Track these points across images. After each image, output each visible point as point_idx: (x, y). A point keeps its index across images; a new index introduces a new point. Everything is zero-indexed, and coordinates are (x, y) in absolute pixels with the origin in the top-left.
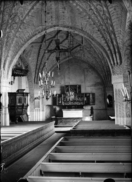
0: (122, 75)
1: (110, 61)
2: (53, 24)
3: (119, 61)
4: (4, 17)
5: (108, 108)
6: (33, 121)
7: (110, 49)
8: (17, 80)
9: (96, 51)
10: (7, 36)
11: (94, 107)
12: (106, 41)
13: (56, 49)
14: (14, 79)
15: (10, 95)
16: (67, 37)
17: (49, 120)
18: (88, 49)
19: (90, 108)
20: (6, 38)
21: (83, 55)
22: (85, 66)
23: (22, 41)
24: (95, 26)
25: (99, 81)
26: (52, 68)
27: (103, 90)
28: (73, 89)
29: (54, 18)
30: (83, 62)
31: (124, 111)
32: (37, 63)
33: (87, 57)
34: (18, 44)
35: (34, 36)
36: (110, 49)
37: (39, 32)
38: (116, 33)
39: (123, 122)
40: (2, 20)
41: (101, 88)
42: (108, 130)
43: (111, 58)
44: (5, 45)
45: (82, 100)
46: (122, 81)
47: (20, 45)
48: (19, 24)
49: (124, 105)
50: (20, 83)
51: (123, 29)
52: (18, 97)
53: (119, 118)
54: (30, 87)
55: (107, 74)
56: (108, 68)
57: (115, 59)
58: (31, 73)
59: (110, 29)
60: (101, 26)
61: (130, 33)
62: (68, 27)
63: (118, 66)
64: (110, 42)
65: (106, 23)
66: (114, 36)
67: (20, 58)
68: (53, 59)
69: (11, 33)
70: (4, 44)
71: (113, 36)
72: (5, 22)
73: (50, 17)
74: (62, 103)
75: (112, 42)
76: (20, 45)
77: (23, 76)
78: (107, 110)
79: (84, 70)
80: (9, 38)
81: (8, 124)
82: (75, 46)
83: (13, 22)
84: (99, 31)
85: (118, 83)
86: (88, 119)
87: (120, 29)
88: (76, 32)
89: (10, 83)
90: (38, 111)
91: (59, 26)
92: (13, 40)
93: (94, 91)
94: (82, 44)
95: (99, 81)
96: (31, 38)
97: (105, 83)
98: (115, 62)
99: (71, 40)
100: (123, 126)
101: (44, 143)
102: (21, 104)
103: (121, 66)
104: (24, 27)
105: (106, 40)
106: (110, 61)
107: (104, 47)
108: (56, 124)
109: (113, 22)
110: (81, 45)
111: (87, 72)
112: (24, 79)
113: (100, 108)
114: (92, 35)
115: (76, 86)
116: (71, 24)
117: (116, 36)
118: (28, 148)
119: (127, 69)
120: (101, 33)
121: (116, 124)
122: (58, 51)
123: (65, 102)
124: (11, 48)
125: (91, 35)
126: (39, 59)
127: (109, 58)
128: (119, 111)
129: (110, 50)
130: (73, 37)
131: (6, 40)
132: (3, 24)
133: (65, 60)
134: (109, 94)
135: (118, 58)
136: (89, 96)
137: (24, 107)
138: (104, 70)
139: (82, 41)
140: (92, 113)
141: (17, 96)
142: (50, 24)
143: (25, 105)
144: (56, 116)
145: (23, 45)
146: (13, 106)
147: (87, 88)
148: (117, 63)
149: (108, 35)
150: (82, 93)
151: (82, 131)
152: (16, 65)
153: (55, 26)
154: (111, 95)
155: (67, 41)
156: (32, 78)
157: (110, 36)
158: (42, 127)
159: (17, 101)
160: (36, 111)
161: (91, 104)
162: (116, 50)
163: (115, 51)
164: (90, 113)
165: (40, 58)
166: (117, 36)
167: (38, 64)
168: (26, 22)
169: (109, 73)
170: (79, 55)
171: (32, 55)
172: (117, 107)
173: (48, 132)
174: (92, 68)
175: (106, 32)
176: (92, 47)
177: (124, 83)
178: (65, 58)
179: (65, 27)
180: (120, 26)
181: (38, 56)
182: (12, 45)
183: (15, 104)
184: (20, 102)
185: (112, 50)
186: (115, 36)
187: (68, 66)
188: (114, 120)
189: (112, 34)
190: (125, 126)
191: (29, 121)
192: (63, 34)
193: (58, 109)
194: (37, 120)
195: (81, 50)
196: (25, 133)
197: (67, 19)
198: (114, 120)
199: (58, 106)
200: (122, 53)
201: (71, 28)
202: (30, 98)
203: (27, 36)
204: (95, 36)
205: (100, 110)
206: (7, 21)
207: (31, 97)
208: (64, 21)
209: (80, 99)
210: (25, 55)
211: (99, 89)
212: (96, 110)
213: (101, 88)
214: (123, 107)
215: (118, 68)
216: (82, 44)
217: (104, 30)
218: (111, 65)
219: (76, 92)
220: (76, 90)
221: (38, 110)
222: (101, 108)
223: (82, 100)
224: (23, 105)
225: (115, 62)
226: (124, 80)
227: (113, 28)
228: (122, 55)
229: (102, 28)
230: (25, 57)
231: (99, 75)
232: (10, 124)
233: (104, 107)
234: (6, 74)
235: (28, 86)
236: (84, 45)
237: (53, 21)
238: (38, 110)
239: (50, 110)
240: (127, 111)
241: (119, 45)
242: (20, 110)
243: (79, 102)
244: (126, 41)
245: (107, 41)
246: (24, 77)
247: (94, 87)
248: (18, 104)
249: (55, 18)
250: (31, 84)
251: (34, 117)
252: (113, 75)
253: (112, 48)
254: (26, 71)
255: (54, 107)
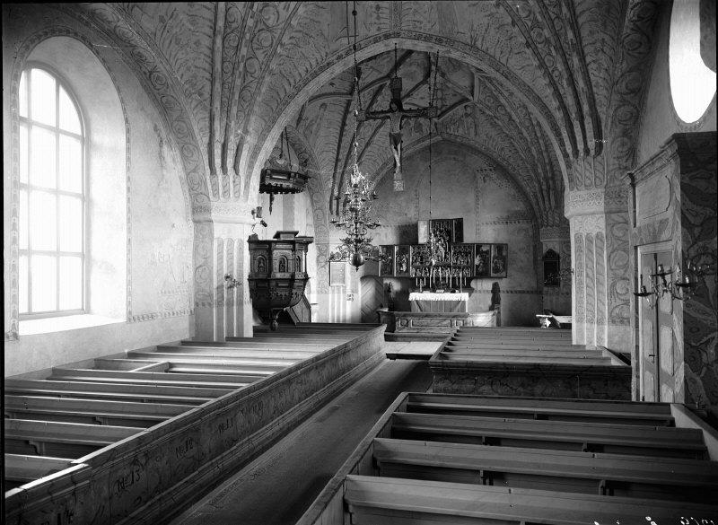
0: (601, 191)
1: (562, 144)
2: (383, 31)
3: (592, 143)
4: (231, 10)
5: (545, 289)
6: (324, 322)
7: (563, 107)
8: (281, 204)
9: (514, 117)
10: (241, 69)
11: (503, 284)
12: (551, 79)
13: (391, 110)
14: (272, 199)
15: (255, 249)
16: (428, 75)
17: (367, 321)
18: (488, 112)
19: (490, 288)
20: (239, 77)
21: (472, 130)
22: (477, 162)
23: (287, 87)
24: (516, 29)
25: (520, 206)
26: (382, 169)
27: (531, 233)
28: (441, 232)
29: (385, 11)
30: (474, 150)
31: (604, 305)
32: (338, 154)
33: (485, 136)
34: (275, 95)
35: (322, 69)
36: (563, 107)
37: (340, 58)
38: (586, 52)
39: (600, 339)
40: (226, 19)
41: (526, 230)
42: (551, 366)
43: (565, 135)
44: (237, 97)
45: (468, 262)
46: (602, 208)
47: (282, 96)
48: (280, 31)
49: (602, 284)
50: (288, 209)
51: (613, 34)
52: (277, 254)
53: (585, 325)
54: (318, 224)
55: (544, 187)
56: (548, 168)
57: (579, 137)
58: (321, 185)
59: (566, 38)
60: (536, 30)
61: (637, 45)
62: (428, 38)
63: (590, 159)
64: (565, 82)
65: (553, 16)
66: (580, 60)
67: (285, 136)
68: (383, 143)
69: (255, 61)
70: (233, 94)
71: (575, 60)
72: (234, 25)
73: (374, 10)
74: (407, 270)
75: (572, 82)
76: (282, 96)
77: (293, 191)
78: (541, 292)
79: (475, 177)
80: (249, 75)
81: (249, 333)
82: (448, 103)
83: (260, 26)
84: (528, 45)
85: (586, 214)
86: (483, 319)
87: (602, 35)
88: (455, 55)
89: (253, 213)
90: (339, 293)
91: (403, 35)
92: (260, 83)
93: (502, 239)
94: (471, 98)
95: (520, 206)
96: (315, 75)
97: (540, 207)
98: (580, 147)
99: (438, 86)
100: (600, 352)
101: (350, 392)
102: (287, 276)
103: (599, 158)
104: (293, 41)
105: (550, 76)
106: (562, 144)
107: (545, 100)
108: (391, 328)
109: (578, 12)
110: (467, 100)
111: (485, 182)
112: (300, 200)
113: (521, 286)
114: (504, 62)
115: (449, 222)
116: (437, 27)
117: (588, 62)
118: (297, 414)
119: (620, 168)
120: (536, 54)
121: (574, 343)
122: (397, 114)
123: (417, 268)
124: (256, 109)
125: (503, 61)
126: (342, 145)
127: (558, 135)
128: (587, 303)
129: (565, 107)
130: (443, 75)
131: (238, 82)
132: (229, 31)
133: (418, 147)
134: (550, 246)
135: (590, 133)
136: (488, 252)
137: (296, 284)
138: (537, 175)
139: (473, 86)
140: (496, 300)
141: (275, 252)
142: (373, 31)
143: (299, 276)
144: (388, 312)
145: (292, 97)
146: (262, 280)
147: (483, 229)
148: (587, 151)
149: (561, 60)
150: (465, 241)
151: (466, 366)
152: (271, 161)
153: (387, 37)
154: (557, 249)
155: (425, 87)
156: (324, 198)
157: (566, 63)
158: (346, 345)
159: (276, 265)
160: (333, 291)
161: (492, 274)
162: (586, 108)
163: (580, 110)
164: (490, 303)
165: (346, 140)
166: (588, 59)
167: (340, 157)
168: (299, 23)
169: (551, 182)
170: (461, 131)
171: (322, 133)
172: (580, 290)
173: (364, 358)
174: (501, 169)
175: (552, 49)
176: (501, 105)
177: (606, 213)
178: (419, 141)
179: (418, 38)
180: (604, 25)
181: (341, 135)
182: (259, 99)
183: (269, 275)
184: (283, 267)
185: (571, 108)
186: (582, 58)
187: (428, 163)
188: (568, 326)
189: (575, 54)
190: (605, 354)
191: (314, 320)
192: (414, 68)
193: (396, 286)
194: (333, 320)
195: (467, 115)
196: (290, 364)
197: (425, 12)
198: (568, 326)
199: (398, 279)
200: (603, 117)
201: (439, 41)
202: (318, 257)
203: (302, 70)
204: (514, 64)
205: (520, 292)
206: (240, 21)
207: (321, 253)
208: (418, 17)
209: (462, 261)
210: (301, 131)
211: (519, 230)
212: (510, 294)
213: (526, 230)
214: (599, 292)
215: (588, 167)
216: (471, 98)
217: (547, 41)
218: (566, 155)
219: (450, 241)
220: (449, 233)
221: (339, 290)
222: (524, 288)
223: (468, 262)
224: (292, 280)
225: (580, 147)
226: (606, 204)
227: (577, 35)
228: (603, 124)
229: (540, 35)
230: (302, 138)
231: (519, 188)
232: (256, 330)
233: (534, 284)
234: (243, 184)
235: (311, 221)
236: (476, 99)
237: (382, 21)
238: (339, 290)
239: (373, 289)
240: (614, 304)
241: (594, 89)
242: (283, 293)
243: (459, 268)
244: (622, 75)
245: (556, 79)
246: (301, 194)
247: (502, 226)
248: (279, 275)
249: (388, 11)
250: (321, 215)
251: (328, 309)
252: (572, 189)
253: (570, 101)
254: (301, 176)
255: (387, 281)
